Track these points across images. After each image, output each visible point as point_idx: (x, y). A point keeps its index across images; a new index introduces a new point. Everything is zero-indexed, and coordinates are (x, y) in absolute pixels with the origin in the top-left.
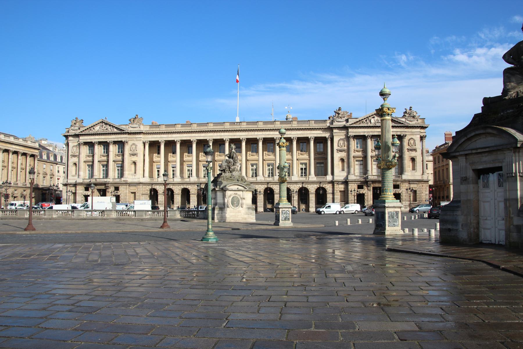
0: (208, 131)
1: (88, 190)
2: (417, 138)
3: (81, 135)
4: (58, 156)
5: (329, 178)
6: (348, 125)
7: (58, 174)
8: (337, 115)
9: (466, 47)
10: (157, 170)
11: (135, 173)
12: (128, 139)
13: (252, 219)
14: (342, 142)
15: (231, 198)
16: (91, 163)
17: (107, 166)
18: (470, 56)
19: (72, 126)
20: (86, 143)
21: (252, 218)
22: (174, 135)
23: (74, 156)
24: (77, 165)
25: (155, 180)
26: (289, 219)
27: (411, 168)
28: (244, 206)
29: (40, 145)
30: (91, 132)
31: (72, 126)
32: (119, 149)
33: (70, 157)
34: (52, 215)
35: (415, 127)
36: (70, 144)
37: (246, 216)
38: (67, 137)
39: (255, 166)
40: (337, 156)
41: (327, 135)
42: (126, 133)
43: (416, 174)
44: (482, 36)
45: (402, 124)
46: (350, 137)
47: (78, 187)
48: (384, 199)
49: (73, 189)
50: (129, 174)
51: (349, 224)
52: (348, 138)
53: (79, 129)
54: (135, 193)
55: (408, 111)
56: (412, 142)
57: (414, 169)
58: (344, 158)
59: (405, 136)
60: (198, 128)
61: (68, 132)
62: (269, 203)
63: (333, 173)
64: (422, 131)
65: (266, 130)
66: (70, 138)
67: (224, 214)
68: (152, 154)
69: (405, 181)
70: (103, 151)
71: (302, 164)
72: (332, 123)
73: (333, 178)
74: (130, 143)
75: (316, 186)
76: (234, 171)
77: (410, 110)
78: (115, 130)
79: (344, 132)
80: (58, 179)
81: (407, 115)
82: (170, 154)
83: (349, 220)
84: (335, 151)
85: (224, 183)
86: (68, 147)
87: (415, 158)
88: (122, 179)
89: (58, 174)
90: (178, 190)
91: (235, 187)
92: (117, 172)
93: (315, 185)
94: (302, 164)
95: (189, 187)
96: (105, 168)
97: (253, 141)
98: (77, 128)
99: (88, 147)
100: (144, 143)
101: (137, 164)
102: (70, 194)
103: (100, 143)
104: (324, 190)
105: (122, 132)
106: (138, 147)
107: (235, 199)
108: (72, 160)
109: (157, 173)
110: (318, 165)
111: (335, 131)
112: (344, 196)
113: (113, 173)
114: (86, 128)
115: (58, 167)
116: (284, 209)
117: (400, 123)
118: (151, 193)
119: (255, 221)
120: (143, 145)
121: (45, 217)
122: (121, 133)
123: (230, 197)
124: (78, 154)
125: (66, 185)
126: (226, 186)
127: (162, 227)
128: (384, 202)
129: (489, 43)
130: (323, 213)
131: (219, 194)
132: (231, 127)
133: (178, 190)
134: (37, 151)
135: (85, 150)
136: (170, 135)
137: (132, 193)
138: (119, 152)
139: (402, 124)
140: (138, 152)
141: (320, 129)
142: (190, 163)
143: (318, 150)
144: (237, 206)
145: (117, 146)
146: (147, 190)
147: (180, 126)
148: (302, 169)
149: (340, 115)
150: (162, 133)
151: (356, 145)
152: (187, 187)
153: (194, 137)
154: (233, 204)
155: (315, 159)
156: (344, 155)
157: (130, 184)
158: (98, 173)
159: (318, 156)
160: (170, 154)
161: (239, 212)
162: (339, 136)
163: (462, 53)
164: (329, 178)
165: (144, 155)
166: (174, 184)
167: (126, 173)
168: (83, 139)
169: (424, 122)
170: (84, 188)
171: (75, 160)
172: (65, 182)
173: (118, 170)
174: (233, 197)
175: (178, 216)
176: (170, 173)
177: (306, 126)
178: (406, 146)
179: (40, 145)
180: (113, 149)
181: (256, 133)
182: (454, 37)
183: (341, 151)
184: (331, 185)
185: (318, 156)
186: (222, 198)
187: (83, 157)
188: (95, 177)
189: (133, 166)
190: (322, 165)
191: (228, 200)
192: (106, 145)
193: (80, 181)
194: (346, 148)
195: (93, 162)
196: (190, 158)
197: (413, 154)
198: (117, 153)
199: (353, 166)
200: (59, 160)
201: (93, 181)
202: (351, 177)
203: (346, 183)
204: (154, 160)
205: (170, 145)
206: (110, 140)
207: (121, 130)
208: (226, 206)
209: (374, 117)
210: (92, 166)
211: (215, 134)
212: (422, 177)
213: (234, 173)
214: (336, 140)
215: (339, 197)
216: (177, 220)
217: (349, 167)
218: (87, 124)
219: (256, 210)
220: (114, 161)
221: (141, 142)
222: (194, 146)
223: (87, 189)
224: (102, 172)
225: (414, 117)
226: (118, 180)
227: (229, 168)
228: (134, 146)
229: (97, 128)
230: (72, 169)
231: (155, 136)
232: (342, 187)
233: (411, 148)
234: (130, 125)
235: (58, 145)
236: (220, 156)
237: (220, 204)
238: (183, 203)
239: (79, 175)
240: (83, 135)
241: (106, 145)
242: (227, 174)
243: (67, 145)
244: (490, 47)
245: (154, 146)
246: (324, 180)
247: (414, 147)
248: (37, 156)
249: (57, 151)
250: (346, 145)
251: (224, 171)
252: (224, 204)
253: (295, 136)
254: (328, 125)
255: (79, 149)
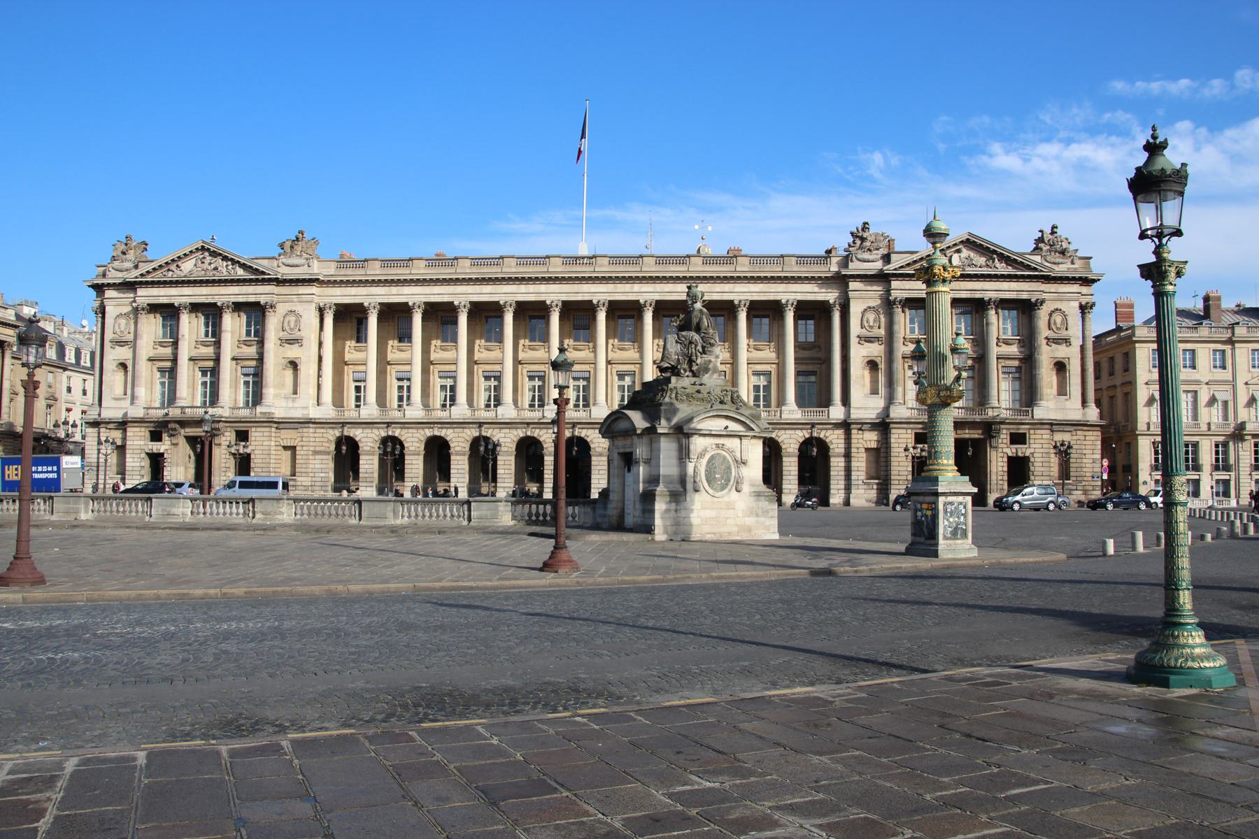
0: (503, 279)
1: (160, 440)
2: (1072, 308)
3: (141, 283)
4: (68, 348)
6: (889, 269)
8: (858, 242)
9: (1010, 139)
10: (353, 385)
11: (295, 393)
12: (275, 299)
13: (767, 528)
14: (871, 316)
15: (704, 461)
16: (168, 364)
17: (215, 372)
19: (114, 259)
20: (154, 308)
21: (766, 528)
23: (120, 343)
24: (130, 368)
25: (351, 414)
26: (965, 535)
28: (746, 488)
29: (18, 317)
30: (170, 276)
31: (114, 259)
33: (107, 344)
34: (77, 512)
35: (1067, 279)
37: (750, 521)
38: (99, 289)
39: (627, 379)
40: (859, 353)
41: (831, 296)
42: (270, 281)
43: (1068, 404)
45: (1035, 269)
46: (894, 302)
47: (131, 431)
48: (935, 473)
49: (117, 435)
50: (276, 396)
51: (1140, 548)
52: (888, 304)
53: (136, 267)
55: (1047, 237)
56: (1058, 318)
57: (1062, 391)
59: (1043, 302)
60: (474, 270)
61: (104, 275)
63: (846, 401)
64: (1084, 290)
66: (110, 293)
67: (683, 514)
68: (339, 342)
69: (1041, 424)
70: (203, 329)
71: (757, 374)
72: (845, 261)
73: (848, 413)
74: (282, 309)
75: (802, 435)
77: (1053, 233)
78: (240, 272)
79: (877, 289)
80: (69, 410)
81: (1045, 248)
82: (390, 342)
83: (1139, 535)
84: (853, 341)
85: (684, 410)
86: (103, 318)
87: (1066, 361)
88: (259, 409)
90: (414, 442)
91: (718, 425)
93: (800, 433)
94: (757, 374)
96: (208, 379)
98: (130, 265)
99: (159, 319)
100: (321, 311)
101: (302, 367)
102: (107, 449)
104: (823, 446)
105: (259, 277)
107: (717, 462)
108: (114, 355)
109: (353, 394)
110: (801, 379)
111: (853, 285)
112: (877, 461)
113: (232, 394)
114: (155, 265)
115: (69, 378)
116: (950, 499)
117: (1028, 267)
118: (338, 447)
119: (776, 536)
121: (54, 518)
122: (257, 281)
123: (701, 455)
124: (131, 337)
125: (95, 424)
126: (690, 420)
127: (546, 567)
128: (935, 480)
129: (1062, 135)
130: (1016, 507)
131: (667, 449)
132: (568, 268)
134: (11, 332)
135: (152, 327)
137: (285, 448)
138: (248, 333)
139: (1035, 269)
140: (302, 333)
143: (802, 339)
144: (723, 488)
145: (244, 317)
146: (329, 441)
148: (757, 388)
149: (867, 244)
151: (908, 326)
154: (710, 480)
155: (798, 361)
156: (876, 350)
157: (280, 424)
159: (806, 354)
160: (390, 342)
161: (730, 506)
162: (863, 299)
163: (1007, 153)
164: (837, 412)
165: (320, 344)
166: (404, 425)
167: (269, 392)
168: (147, 295)
169: (1087, 267)
170: (148, 434)
172: (93, 415)
173: (247, 383)
174: (712, 458)
175: (506, 517)
176: (392, 395)
177: (776, 271)
178: (1043, 332)
179: (18, 317)
180: (233, 325)
181: (637, 287)
183: (869, 340)
184: (840, 432)
185: (806, 354)
186: (674, 461)
187: (146, 347)
188: (180, 403)
189: (289, 373)
191: (697, 467)
192: (212, 313)
193: (137, 412)
194: (882, 332)
195: (175, 360)
197: (1061, 352)
198: (244, 337)
199: (901, 382)
200: (70, 357)
201: (174, 413)
202: (898, 412)
203: (883, 426)
204: (348, 357)
205: (395, 316)
207: (256, 271)
208: (689, 486)
209: (958, 251)
210: (171, 372)
211: (523, 288)
212: (1084, 415)
213: (706, 378)
214: (856, 309)
216: (505, 532)
217: (890, 383)
218: (158, 254)
221: (314, 305)
222: (463, 320)
223: (156, 436)
224: (200, 389)
225: (1063, 252)
226: (245, 413)
228: (292, 319)
229: (188, 266)
232: (871, 439)
233: (1056, 336)
234: (283, 259)
235: (72, 322)
236: (532, 349)
237: (669, 481)
238: (428, 479)
239: (133, 398)
240: (147, 283)
241: (212, 313)
243: (102, 311)
244: (1068, 142)
245: (349, 319)
246: (823, 418)
247: (1064, 334)
248: (10, 345)
249: (65, 334)
250: (883, 325)
252: (683, 480)
253: (743, 297)
254: (834, 268)
255: (136, 323)
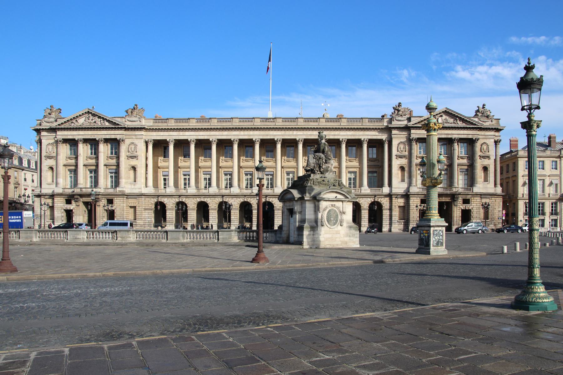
2: (491, 142)
3: (59, 129)
5: (386, 190)
6: (410, 124)
7: (26, 183)
8: (396, 112)
9: (466, 64)
10: (163, 178)
11: (135, 181)
12: (124, 137)
13: (354, 242)
14: (402, 146)
15: (326, 212)
18: (472, 74)
19: (45, 117)
20: (65, 141)
21: (354, 242)
22: (187, 133)
23: (50, 157)
25: (162, 191)
27: (482, 179)
28: (345, 224)
30: (73, 125)
31: (45, 117)
32: (112, 149)
34: (32, 238)
36: (43, 141)
37: (346, 239)
38: (38, 131)
39: (291, 175)
40: (396, 163)
41: (384, 137)
42: (121, 128)
43: (488, 186)
44: (482, 54)
45: (475, 124)
47: (56, 199)
49: (49, 201)
50: (126, 183)
51: (518, 250)
52: (410, 141)
53: (56, 121)
54: (134, 207)
55: (481, 109)
56: (485, 147)
57: (486, 180)
58: (405, 166)
59: (478, 139)
61: (40, 125)
62: (247, 221)
63: (390, 185)
64: (497, 134)
65: (308, 128)
66: (43, 133)
67: (316, 236)
68: (156, 158)
69: (476, 195)
70: (90, 151)
71: (350, 172)
73: (391, 190)
74: (127, 142)
76: (327, 171)
77: (483, 108)
78: (107, 124)
79: (405, 134)
80: (25, 189)
81: (480, 115)
82: (180, 158)
84: (394, 157)
85: (317, 189)
86: (41, 145)
87: (488, 166)
88: (118, 189)
89: (26, 183)
90: (192, 204)
91: (332, 196)
92: (109, 180)
93: (369, 199)
94: (350, 172)
95: (208, 200)
96: (93, 175)
97: (288, 143)
98: (53, 120)
99: (68, 146)
100: (147, 143)
101: (138, 169)
102: (45, 208)
103: (86, 141)
104: (380, 205)
105: (116, 127)
106: (137, 147)
107: (332, 213)
108: (47, 163)
109: (163, 182)
110: (370, 175)
111: (394, 132)
112: (404, 212)
113: (105, 182)
114: (65, 120)
115: (25, 174)
116: (436, 228)
117: (472, 124)
119: (358, 246)
120: (145, 144)
121: (20, 241)
122: (115, 128)
123: (325, 210)
124: (55, 155)
125: (39, 196)
126: (320, 193)
127: (254, 261)
128: (429, 220)
129: (488, 62)
130: (465, 232)
131: (309, 207)
132: (263, 124)
133: (192, 204)
135: (65, 150)
136: (181, 133)
137: (131, 207)
138: (112, 153)
139: (475, 124)
140: (138, 154)
141: (376, 129)
142: (207, 170)
143: (370, 156)
144: (334, 224)
145: (109, 146)
147: (195, 121)
148: (350, 179)
149: (400, 113)
150: (171, 130)
151: (418, 150)
152: (205, 200)
153: (214, 136)
155: (369, 166)
156: (404, 162)
157: (128, 196)
158: (84, 181)
159: (372, 163)
161: (338, 232)
162: (399, 138)
163: (464, 70)
164: (386, 190)
165: (147, 158)
167: (123, 181)
168: (62, 135)
169: (498, 124)
170: (65, 201)
171: (52, 162)
172: (37, 192)
173: (112, 177)
174: (330, 211)
175: (235, 238)
176: (181, 182)
178: (478, 153)
180: (104, 150)
181: (295, 133)
182: (455, 55)
183: (401, 157)
185: (372, 163)
186: (312, 212)
188: (80, 186)
189: (132, 172)
190: (377, 176)
191: (323, 215)
192: (94, 143)
193: (59, 190)
194: (407, 153)
195: (76, 166)
196: (208, 164)
198: (110, 155)
199: (415, 176)
200: (25, 164)
201: (77, 191)
202: (413, 190)
203: (407, 196)
204: (160, 165)
205: (182, 146)
206: (100, 137)
208: (319, 224)
209: (441, 116)
210: (75, 172)
211: (242, 133)
212: (495, 190)
213: (327, 175)
214: (395, 143)
215: (398, 213)
216: (235, 245)
217: (410, 177)
218: (67, 115)
219: (360, 231)
220: (105, 165)
222: (214, 147)
223: (68, 202)
224: (89, 179)
225: (488, 117)
226: (111, 191)
227: (320, 167)
228: (133, 147)
229: (81, 121)
230: (47, 175)
231: (162, 133)
232: (401, 202)
234: (128, 118)
237: (310, 221)
238: (199, 221)
239: (57, 184)
240: (62, 129)
241: (94, 143)
242: (316, 177)
243: (40, 142)
244: (491, 65)
245: (160, 146)
246: (380, 193)
247: (487, 154)
249: (22, 153)
250: (407, 150)
251: (312, 171)
252: (316, 221)
254: (385, 124)
255: (57, 148)
